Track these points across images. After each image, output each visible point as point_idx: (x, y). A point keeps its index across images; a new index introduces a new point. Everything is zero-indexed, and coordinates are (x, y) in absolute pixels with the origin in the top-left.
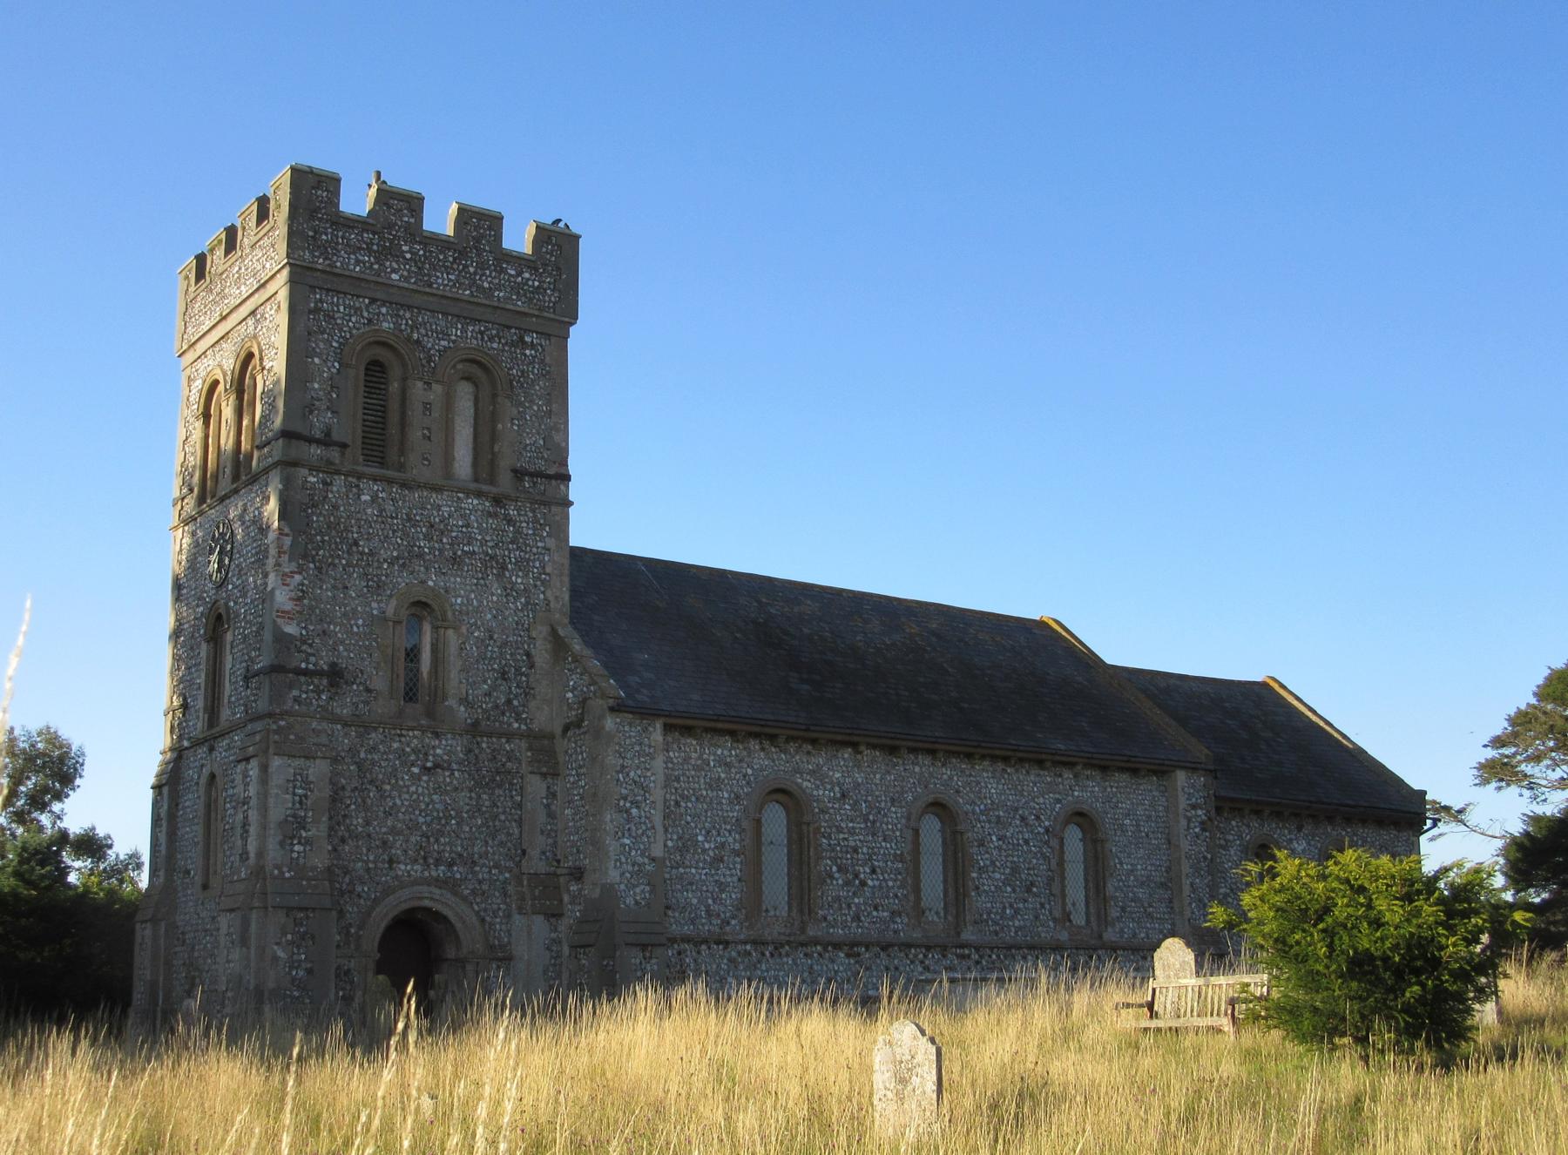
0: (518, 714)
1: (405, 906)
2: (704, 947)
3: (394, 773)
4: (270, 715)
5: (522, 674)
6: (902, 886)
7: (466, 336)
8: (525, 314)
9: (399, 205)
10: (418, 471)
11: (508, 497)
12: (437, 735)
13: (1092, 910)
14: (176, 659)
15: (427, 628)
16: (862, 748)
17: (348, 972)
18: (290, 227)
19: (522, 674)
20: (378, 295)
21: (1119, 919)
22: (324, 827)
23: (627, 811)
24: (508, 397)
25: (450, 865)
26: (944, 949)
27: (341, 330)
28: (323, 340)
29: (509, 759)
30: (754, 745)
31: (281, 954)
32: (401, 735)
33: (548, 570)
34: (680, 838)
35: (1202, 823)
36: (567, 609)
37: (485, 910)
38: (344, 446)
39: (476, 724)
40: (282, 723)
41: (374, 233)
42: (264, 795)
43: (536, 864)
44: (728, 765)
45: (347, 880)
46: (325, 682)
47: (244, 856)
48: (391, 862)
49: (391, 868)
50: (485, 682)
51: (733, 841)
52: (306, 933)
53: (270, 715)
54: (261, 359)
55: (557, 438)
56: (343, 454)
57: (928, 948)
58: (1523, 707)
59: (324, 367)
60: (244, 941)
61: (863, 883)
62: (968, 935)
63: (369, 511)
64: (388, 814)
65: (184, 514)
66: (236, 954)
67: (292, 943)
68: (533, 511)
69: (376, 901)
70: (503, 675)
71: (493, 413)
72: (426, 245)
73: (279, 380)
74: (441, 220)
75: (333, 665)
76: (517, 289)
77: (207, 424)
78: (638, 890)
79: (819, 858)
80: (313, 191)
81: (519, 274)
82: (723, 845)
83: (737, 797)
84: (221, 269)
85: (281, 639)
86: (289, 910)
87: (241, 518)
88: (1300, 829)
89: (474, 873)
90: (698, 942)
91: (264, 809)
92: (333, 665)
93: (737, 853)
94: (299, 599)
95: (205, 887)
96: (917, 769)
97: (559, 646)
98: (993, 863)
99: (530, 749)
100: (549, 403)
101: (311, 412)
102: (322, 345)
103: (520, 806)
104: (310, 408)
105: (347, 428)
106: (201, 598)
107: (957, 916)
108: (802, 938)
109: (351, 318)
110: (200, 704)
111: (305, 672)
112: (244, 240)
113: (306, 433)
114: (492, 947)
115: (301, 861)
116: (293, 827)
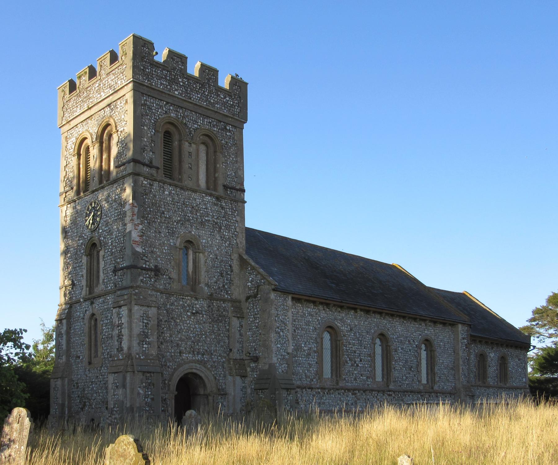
0: (227, 292)
1: (186, 372)
2: (304, 390)
3: (181, 315)
4: (132, 287)
5: (228, 274)
6: (370, 367)
7: (203, 123)
8: (227, 116)
9: (177, 59)
10: (187, 183)
11: (221, 197)
12: (197, 299)
13: (429, 378)
14: (66, 264)
15: (191, 252)
16: (358, 310)
17: (165, 400)
18: (133, 63)
19: (228, 274)
20: (170, 101)
21: (439, 381)
22: (155, 337)
23: (279, 333)
24: (221, 153)
25: (203, 355)
26: (384, 392)
27: (155, 115)
29: (224, 310)
30: (321, 307)
31: (141, 392)
32: (183, 299)
33: (237, 230)
34: (296, 345)
35: (466, 345)
36: (244, 248)
37: (216, 374)
38: (158, 168)
39: (212, 295)
40: (137, 291)
41: (168, 71)
42: (130, 322)
43: (235, 355)
44: (312, 315)
46: (153, 273)
47: (120, 349)
48: (180, 353)
49: (180, 356)
50: (215, 277)
51: (314, 346)
52: (151, 383)
53: (132, 287)
54: (116, 127)
55: (240, 173)
56: (157, 172)
57: (379, 391)
58: (539, 307)
59: (148, 131)
60: (124, 386)
61: (357, 365)
62: (391, 387)
63: (168, 199)
64: (179, 332)
65: (67, 200)
66: (120, 391)
67: (145, 387)
68: (231, 204)
69: (175, 370)
70: (221, 274)
72: (188, 80)
73: (129, 135)
74: (194, 69)
75: (156, 266)
76: (224, 104)
77: (79, 158)
78: (283, 366)
79: (343, 355)
80: (142, 48)
81: (225, 98)
82: (311, 348)
83: (315, 329)
84: (86, 86)
85: (135, 253)
86: (144, 372)
87: (107, 200)
88: (492, 348)
89: (212, 358)
90: (302, 388)
91: (130, 329)
92: (156, 266)
93: (315, 352)
94: (141, 236)
95: (90, 363)
96: (375, 320)
97: (243, 263)
98: (399, 358)
99: (232, 306)
100: (236, 157)
101: (144, 151)
102: (147, 121)
103: (228, 330)
104: (143, 150)
105: (158, 161)
107: (387, 379)
108: (338, 387)
109: (160, 111)
110: (84, 283)
111: (145, 269)
112: (102, 72)
113: (142, 161)
114: (219, 390)
115: (147, 352)
116: (144, 336)
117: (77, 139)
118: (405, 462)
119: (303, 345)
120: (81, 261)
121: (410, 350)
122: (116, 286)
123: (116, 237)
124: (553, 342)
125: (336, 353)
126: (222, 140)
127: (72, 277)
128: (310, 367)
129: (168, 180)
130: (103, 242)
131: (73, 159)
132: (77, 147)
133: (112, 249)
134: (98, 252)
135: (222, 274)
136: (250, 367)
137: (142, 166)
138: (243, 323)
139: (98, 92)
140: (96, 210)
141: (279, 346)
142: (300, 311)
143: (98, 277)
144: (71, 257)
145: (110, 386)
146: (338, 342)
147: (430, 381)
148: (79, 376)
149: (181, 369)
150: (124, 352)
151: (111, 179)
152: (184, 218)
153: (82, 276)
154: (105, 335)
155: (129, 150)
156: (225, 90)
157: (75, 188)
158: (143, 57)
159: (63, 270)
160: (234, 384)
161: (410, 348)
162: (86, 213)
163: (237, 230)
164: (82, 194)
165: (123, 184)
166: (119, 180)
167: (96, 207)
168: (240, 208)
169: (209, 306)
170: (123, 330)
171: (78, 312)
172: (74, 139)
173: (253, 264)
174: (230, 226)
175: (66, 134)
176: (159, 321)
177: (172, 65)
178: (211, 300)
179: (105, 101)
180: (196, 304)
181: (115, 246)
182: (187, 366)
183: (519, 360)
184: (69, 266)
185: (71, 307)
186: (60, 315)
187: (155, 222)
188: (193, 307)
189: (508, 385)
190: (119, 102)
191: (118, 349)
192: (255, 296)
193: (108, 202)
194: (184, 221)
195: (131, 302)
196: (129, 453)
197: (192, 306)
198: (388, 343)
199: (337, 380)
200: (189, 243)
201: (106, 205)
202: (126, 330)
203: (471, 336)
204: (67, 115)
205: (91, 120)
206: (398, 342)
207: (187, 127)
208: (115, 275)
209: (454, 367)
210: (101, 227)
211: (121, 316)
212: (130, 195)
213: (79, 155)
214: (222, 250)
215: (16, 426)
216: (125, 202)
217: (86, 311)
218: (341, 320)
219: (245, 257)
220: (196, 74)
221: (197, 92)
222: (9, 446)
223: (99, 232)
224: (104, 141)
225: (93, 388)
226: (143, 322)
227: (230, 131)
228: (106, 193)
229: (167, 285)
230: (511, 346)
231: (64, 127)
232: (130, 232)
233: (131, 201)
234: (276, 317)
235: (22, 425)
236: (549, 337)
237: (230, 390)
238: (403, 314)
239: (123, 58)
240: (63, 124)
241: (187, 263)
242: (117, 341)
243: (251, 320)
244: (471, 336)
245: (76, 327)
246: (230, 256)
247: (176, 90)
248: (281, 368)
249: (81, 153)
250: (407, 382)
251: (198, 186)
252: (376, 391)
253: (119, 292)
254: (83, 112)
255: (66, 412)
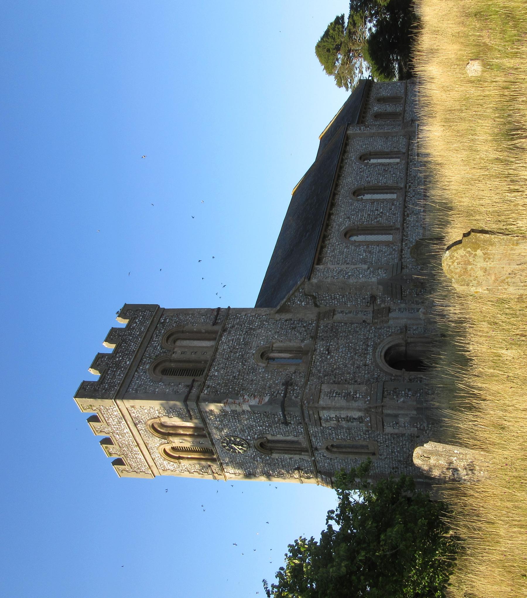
0: (309, 324)
1: (384, 361)
4: (302, 406)
5: (294, 323)
6: (383, 202)
7: (157, 342)
9: (99, 362)
10: (208, 356)
11: (223, 327)
12: (315, 350)
14: (280, 475)
15: (272, 355)
16: (331, 212)
17: (410, 380)
18: (99, 398)
20: (135, 369)
22: (350, 386)
23: (349, 276)
24: (184, 327)
25: (368, 346)
27: (146, 382)
28: (149, 388)
30: (327, 242)
31: (402, 399)
32: (314, 362)
34: (361, 263)
35: (366, 127)
36: (270, 309)
37: (386, 335)
39: (312, 337)
40: (305, 402)
42: (335, 409)
43: (369, 317)
45: (372, 380)
46: (290, 387)
47: (360, 420)
50: (295, 334)
52: (393, 391)
53: (302, 406)
54: (155, 418)
55: (203, 312)
56: (197, 381)
58: (335, 82)
60: (396, 416)
61: (382, 213)
62: (402, 185)
63: (222, 372)
64: (346, 366)
65: (220, 473)
67: (397, 396)
69: (381, 370)
70: (294, 328)
71: (189, 332)
72: (117, 352)
73: (162, 404)
74: (109, 347)
76: (141, 323)
79: (371, 224)
81: (136, 323)
82: (364, 251)
83: (347, 247)
84: (118, 448)
85: (270, 402)
86: (383, 397)
87: (221, 430)
88: (369, 108)
89: (371, 338)
91: (341, 408)
92: (283, 384)
93: (368, 247)
94: (255, 397)
95: (374, 454)
97: (283, 310)
100: (189, 314)
101: (178, 392)
103: (346, 324)
104: (176, 392)
105: (188, 380)
106: (254, 459)
107: (394, 189)
110: (297, 457)
114: (401, 333)
115: (363, 394)
116: (348, 397)
117: (165, 459)
118: (473, 68)
119: (361, 257)
120: (277, 459)
121: (369, 171)
122: (301, 423)
123: (255, 421)
124: (366, 71)
125: (369, 230)
126: (173, 326)
127: (291, 470)
128: (382, 251)
129: (206, 371)
130: (259, 435)
131: (183, 465)
132: (172, 460)
133: (266, 426)
134: (269, 441)
135: (293, 328)
136: (380, 304)
137: (191, 394)
138: (340, 310)
139: (124, 436)
140: (229, 442)
141: (361, 276)
142: (330, 259)
143: (292, 442)
144: (273, 471)
145: (396, 431)
146: (359, 228)
147: (398, 156)
148: (387, 466)
149: (381, 365)
150: (363, 415)
151: (201, 425)
152: (240, 359)
153: (290, 459)
154: (347, 437)
155: (175, 405)
156: (129, 322)
157: (209, 463)
158: (95, 390)
159: (285, 479)
160: (397, 318)
161: (367, 171)
162: (233, 452)
163: (254, 314)
164: (215, 456)
165: (206, 412)
166: (203, 417)
167: (227, 441)
168: (234, 311)
169: (323, 339)
170: (342, 416)
171: (324, 464)
172: (165, 462)
173: (285, 300)
174: (249, 321)
175: (161, 471)
176: (334, 382)
177: (104, 365)
178: (317, 338)
179: (131, 428)
180: (320, 351)
181: (263, 422)
182: (379, 361)
183: (381, 88)
184: (281, 473)
185: (320, 472)
186: (327, 484)
187: (242, 384)
188: (323, 353)
189: (403, 96)
190: (133, 415)
191: (360, 422)
192: (314, 298)
193: (222, 429)
194: (243, 359)
195: (315, 407)
196: (462, 257)
197: (321, 355)
198: (362, 189)
199: (395, 229)
200: (264, 355)
201: (225, 431)
202: (342, 412)
203: (358, 123)
204: (143, 469)
205: (148, 444)
206: (361, 181)
207: (159, 353)
208: (290, 423)
209: (385, 136)
210: (245, 437)
211: (328, 418)
212: (217, 406)
213: (179, 458)
214: (271, 328)
215: (432, 461)
216: (222, 410)
217: (323, 456)
218: (339, 226)
219: (278, 307)
220: (113, 346)
221: (129, 345)
222: (455, 470)
223: (250, 440)
224: (167, 432)
225: (398, 452)
226: (335, 397)
227: (165, 320)
228: (214, 431)
229: (301, 375)
230: (368, 94)
231: (154, 472)
232: (250, 406)
233: (222, 405)
234: (334, 278)
235: (431, 453)
236: (362, 74)
237: (403, 322)
238: (336, 177)
239: (94, 408)
240: (151, 472)
241: (282, 358)
242: (352, 422)
243: (336, 302)
244: (358, 123)
245: (339, 467)
246: (277, 321)
247: (126, 363)
248: (382, 274)
249: (178, 456)
250: (398, 173)
251: (212, 346)
252: (405, 199)
253: (306, 420)
254: (141, 452)
255: (422, 480)
